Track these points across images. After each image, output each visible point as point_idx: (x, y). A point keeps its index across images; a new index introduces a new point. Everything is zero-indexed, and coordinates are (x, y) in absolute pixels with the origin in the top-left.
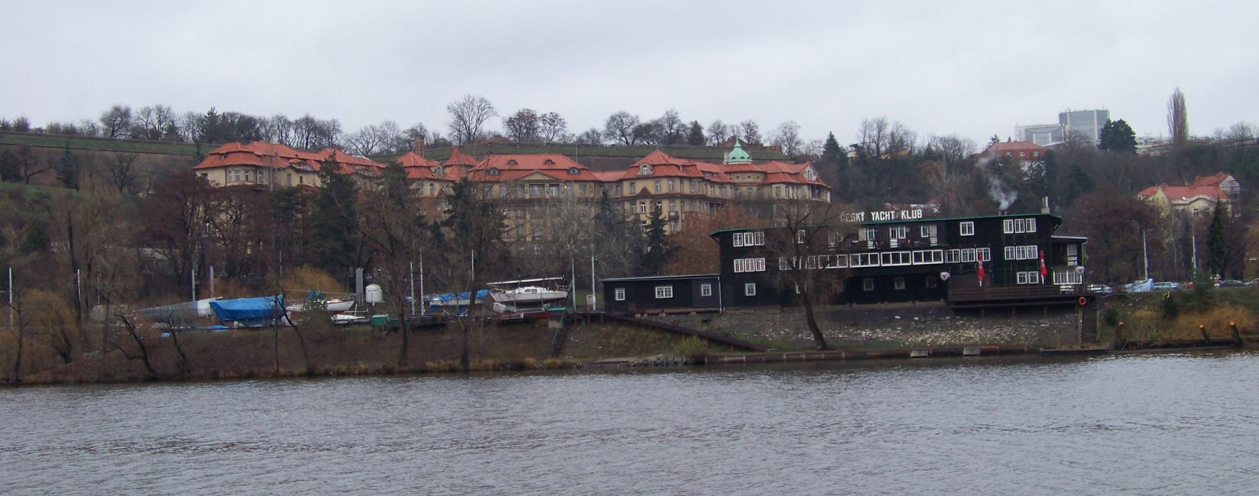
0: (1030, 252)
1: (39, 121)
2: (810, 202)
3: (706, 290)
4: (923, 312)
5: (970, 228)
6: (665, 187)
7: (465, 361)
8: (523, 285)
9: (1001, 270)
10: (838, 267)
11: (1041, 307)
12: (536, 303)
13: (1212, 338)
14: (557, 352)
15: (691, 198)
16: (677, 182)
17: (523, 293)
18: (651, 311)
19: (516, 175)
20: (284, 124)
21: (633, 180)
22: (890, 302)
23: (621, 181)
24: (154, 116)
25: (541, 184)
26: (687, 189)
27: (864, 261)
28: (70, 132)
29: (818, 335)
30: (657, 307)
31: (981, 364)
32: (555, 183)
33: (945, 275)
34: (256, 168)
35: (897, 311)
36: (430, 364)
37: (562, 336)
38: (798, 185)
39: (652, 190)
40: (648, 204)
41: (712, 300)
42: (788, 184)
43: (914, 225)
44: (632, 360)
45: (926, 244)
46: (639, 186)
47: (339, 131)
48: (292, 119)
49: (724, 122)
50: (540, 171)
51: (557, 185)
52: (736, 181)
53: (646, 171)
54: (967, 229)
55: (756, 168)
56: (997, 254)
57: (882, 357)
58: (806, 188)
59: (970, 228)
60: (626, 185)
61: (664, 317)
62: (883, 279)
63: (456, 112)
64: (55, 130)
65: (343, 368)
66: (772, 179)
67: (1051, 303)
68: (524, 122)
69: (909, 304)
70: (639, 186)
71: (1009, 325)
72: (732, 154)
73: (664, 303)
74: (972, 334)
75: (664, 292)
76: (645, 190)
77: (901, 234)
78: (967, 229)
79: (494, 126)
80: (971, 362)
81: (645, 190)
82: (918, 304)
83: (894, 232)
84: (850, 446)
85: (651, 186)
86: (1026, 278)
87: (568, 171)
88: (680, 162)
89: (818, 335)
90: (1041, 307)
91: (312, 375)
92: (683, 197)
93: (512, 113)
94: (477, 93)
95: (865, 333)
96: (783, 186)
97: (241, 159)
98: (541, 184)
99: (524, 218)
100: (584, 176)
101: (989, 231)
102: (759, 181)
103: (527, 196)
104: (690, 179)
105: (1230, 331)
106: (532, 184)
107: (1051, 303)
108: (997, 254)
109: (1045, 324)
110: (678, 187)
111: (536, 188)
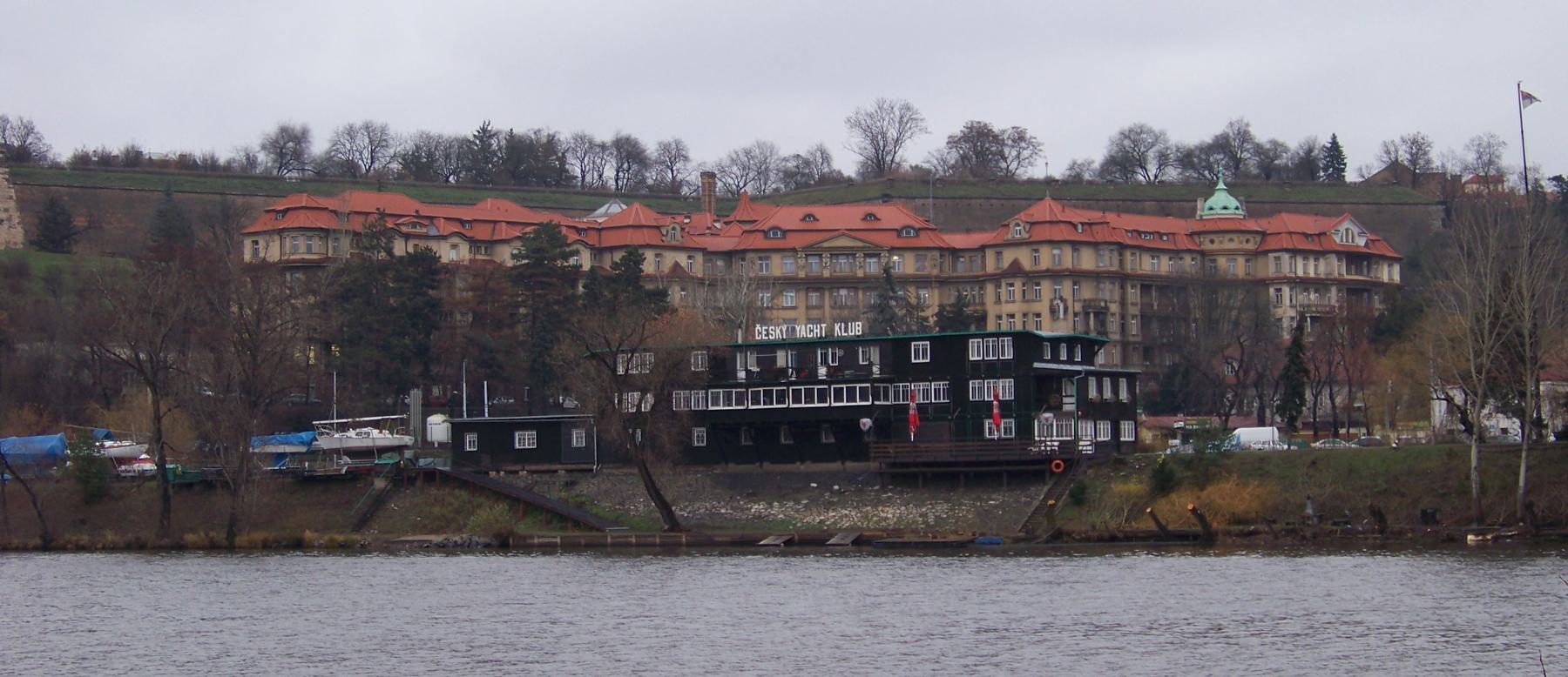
0: (1004, 388)
1: (158, 145)
2: (1340, 283)
3: (578, 439)
4: (851, 478)
5: (924, 351)
6: (1046, 258)
7: (231, 535)
8: (355, 426)
9: (968, 415)
10: (803, 405)
11: (998, 475)
12: (367, 453)
13: (1170, 528)
14: (362, 523)
15: (1097, 276)
16: (1068, 250)
17: (353, 439)
18: (534, 468)
19: (810, 239)
20: (590, 147)
21: (999, 247)
22: (815, 461)
23: (983, 248)
24: (363, 141)
25: (850, 253)
26: (1087, 260)
27: (781, 397)
28: (209, 168)
29: (665, 507)
30: (515, 462)
31: (784, 554)
32: (873, 252)
33: (866, 422)
34: (325, 233)
35: (811, 477)
36: (190, 538)
37: (380, 501)
38: (1319, 254)
39: (1027, 264)
40: (1018, 284)
41: (584, 454)
42: (1294, 252)
43: (850, 345)
44: (437, 539)
45: (864, 374)
46: (1008, 256)
47: (686, 158)
48: (598, 139)
49: (1388, 139)
50: (850, 232)
51: (878, 255)
52: (1207, 246)
53: (1017, 231)
54: (921, 353)
55: (1252, 225)
56: (958, 391)
57: (1100, 539)
58: (1333, 259)
59: (924, 351)
60: (990, 255)
61: (523, 477)
62: (806, 427)
63: (866, 130)
64: (185, 164)
65: (85, 539)
66: (1272, 243)
67: (1022, 468)
68: (981, 147)
69: (835, 466)
70: (1008, 256)
71: (947, 501)
72: (1211, 202)
73: (525, 456)
74: (892, 513)
75: (525, 440)
76: (1016, 263)
77: (834, 356)
78: (921, 353)
79: (921, 151)
80: (841, 551)
81: (1016, 263)
82: (849, 464)
83: (824, 356)
84: (962, 661)
85: (1024, 257)
86: (997, 430)
87: (898, 232)
88: (1079, 216)
89: (665, 507)
90: (998, 475)
91: (48, 546)
92: (1077, 276)
93: (957, 129)
94: (897, 95)
95: (757, 508)
96: (1286, 257)
97: (302, 220)
98: (850, 253)
99: (820, 307)
100: (925, 240)
101: (949, 357)
102: (1251, 246)
103: (826, 274)
104: (1096, 245)
105: (1193, 519)
106: (836, 253)
107: (1022, 468)
108: (958, 391)
109: (994, 500)
110: (1067, 259)
111: (842, 260)
